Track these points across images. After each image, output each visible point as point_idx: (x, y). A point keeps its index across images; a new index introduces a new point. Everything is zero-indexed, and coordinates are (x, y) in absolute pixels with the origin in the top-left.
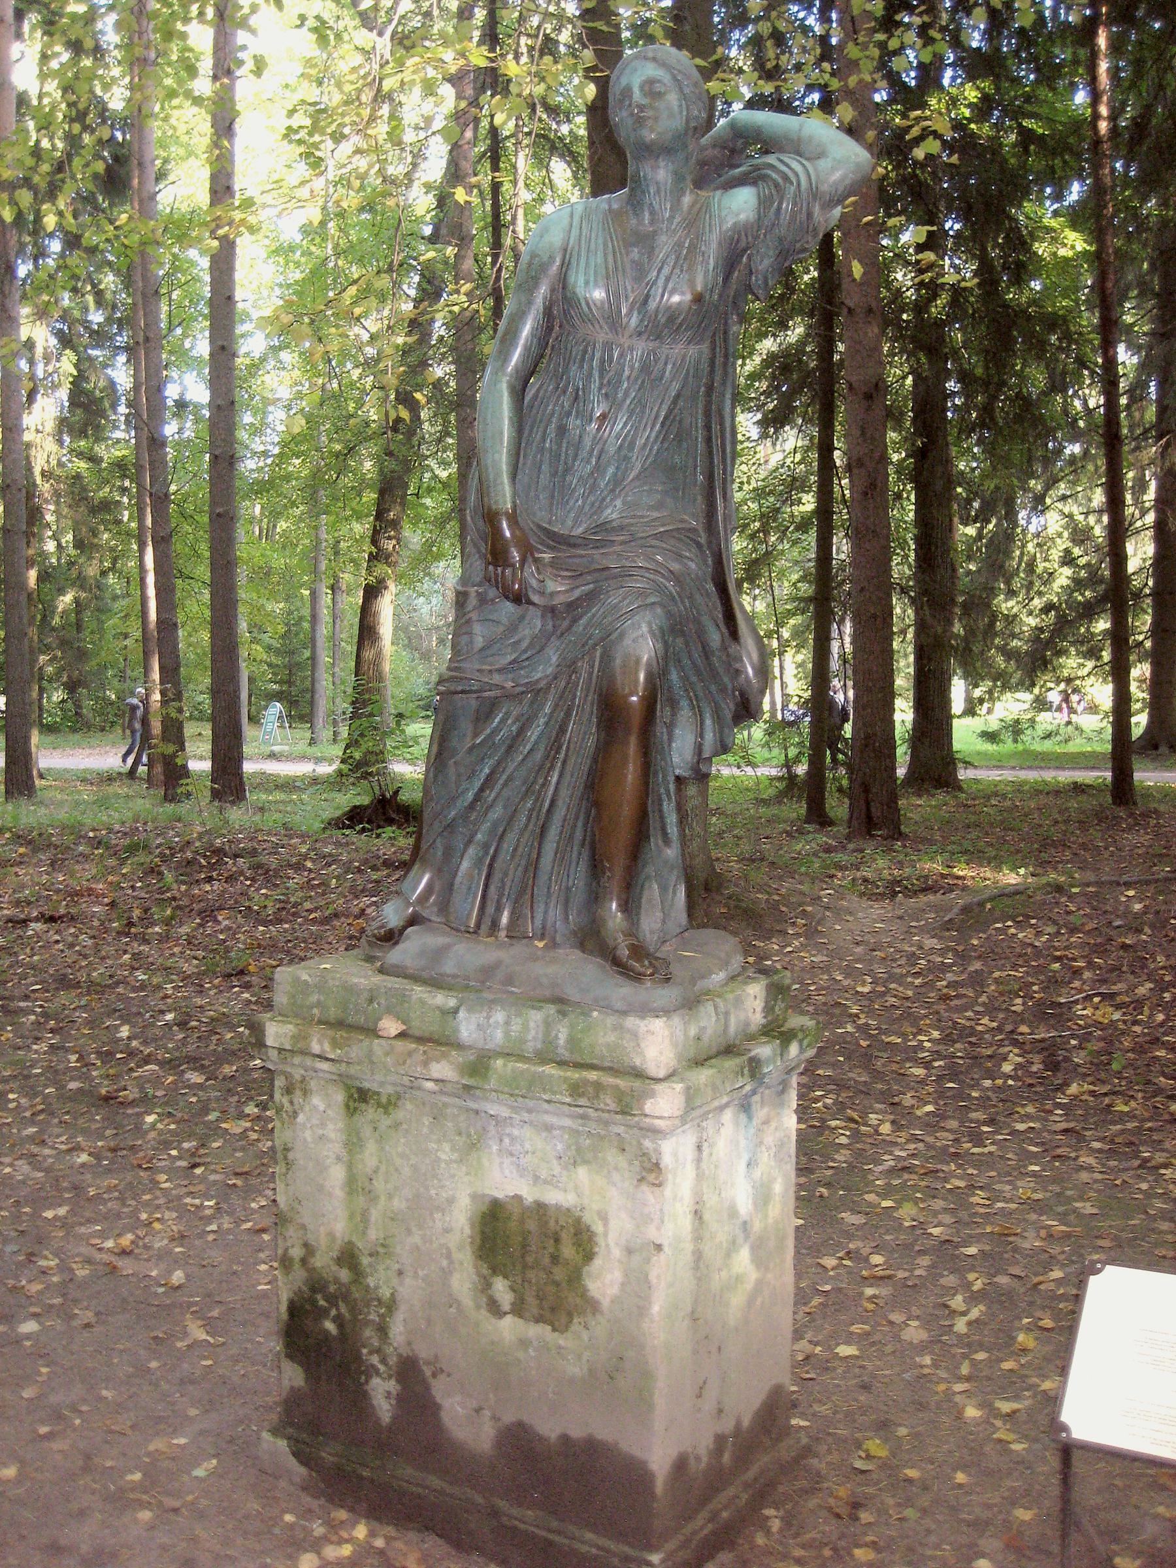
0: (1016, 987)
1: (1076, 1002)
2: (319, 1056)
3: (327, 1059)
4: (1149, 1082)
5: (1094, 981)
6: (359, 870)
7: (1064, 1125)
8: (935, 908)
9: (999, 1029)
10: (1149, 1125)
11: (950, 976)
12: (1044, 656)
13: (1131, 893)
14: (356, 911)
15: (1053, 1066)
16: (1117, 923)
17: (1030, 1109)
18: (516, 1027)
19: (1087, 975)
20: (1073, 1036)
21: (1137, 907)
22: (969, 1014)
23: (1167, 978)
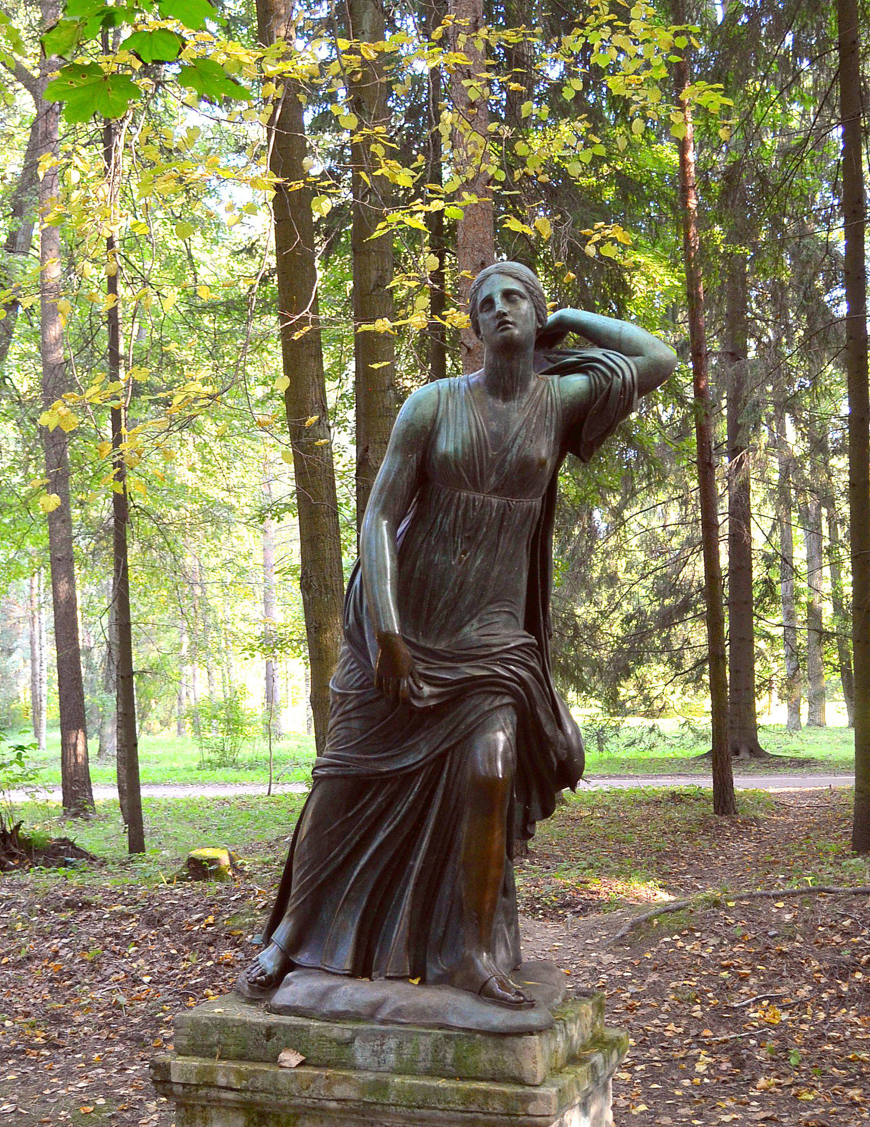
0: (693, 995)
1: (748, 1006)
2: (223, 1088)
3: (232, 1090)
4: (824, 1073)
5: (760, 986)
6: (43, 913)
7: (763, 1115)
8: (606, 926)
9: (686, 1033)
10: (834, 1109)
11: (631, 988)
12: (627, 665)
13: (781, 905)
14: (50, 953)
15: (740, 1064)
16: (772, 933)
17: (729, 1103)
18: (408, 1049)
19: (753, 981)
20: (752, 1036)
21: (788, 917)
22: (656, 1021)
23: (823, 981)
